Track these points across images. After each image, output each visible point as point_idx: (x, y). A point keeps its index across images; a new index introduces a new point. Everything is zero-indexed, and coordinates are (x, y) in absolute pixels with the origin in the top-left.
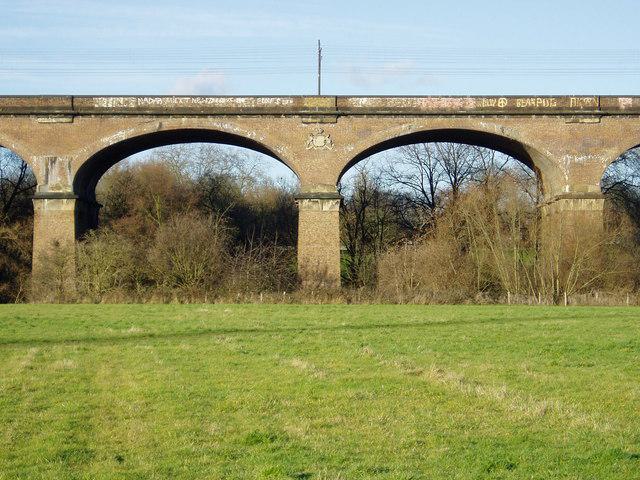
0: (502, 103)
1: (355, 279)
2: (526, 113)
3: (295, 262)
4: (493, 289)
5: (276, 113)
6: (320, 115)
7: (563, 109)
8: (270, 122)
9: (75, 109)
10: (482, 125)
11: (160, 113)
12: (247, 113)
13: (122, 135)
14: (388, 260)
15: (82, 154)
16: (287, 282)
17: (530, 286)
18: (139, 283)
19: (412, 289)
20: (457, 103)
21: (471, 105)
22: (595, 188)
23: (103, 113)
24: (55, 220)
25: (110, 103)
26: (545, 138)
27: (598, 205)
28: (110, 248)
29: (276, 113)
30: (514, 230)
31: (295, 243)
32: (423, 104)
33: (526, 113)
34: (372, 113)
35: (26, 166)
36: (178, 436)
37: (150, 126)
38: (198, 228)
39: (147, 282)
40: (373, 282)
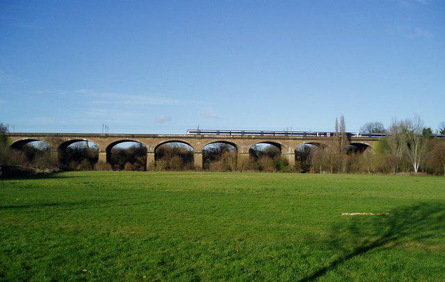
1: (205, 167)
3: (280, 156)
4: (230, 169)
9: (155, 136)
11: (170, 137)
13: (163, 141)
14: (213, 165)
15: (156, 145)
16: (193, 168)
17: (236, 169)
18: (168, 168)
19: (216, 170)
22: (248, 152)
23: (160, 137)
24: (151, 157)
28: (161, 162)
30: (291, 158)
35: (379, 169)
37: (169, 140)
38: (177, 158)
39: (169, 168)
40: (208, 168)
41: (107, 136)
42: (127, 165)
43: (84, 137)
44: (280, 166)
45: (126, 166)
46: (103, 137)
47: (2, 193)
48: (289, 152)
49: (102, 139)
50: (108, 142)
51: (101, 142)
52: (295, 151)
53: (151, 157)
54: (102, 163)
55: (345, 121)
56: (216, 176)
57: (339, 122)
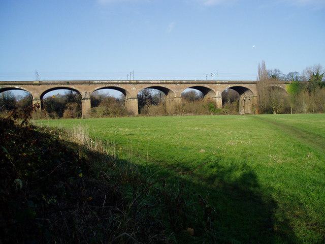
0: (164, 82)
1: (93, 113)
2: (168, 83)
5: (126, 83)
6: (134, 84)
7: (175, 83)
8: (125, 85)
9: (90, 83)
10: (117, 86)
11: (102, 83)
12: (121, 83)
20: (157, 82)
21: (159, 82)
22: (180, 96)
23: (95, 84)
25: (218, 82)
26: (172, 88)
27: (180, 99)
29: (126, 83)
30: (219, 101)
31: (81, 109)
32: (151, 82)
33: (168, 83)
34: (143, 83)
36: (138, 156)
41: (40, 83)
42: (156, 115)
43: (15, 84)
44: (212, 108)
45: (65, 114)
46: (36, 84)
47: (103, 243)
48: (217, 95)
49: (36, 87)
50: (42, 89)
51: (34, 89)
52: (222, 94)
53: (86, 105)
54: (219, 110)
55: (266, 65)
56: (293, 120)
57: (261, 64)
